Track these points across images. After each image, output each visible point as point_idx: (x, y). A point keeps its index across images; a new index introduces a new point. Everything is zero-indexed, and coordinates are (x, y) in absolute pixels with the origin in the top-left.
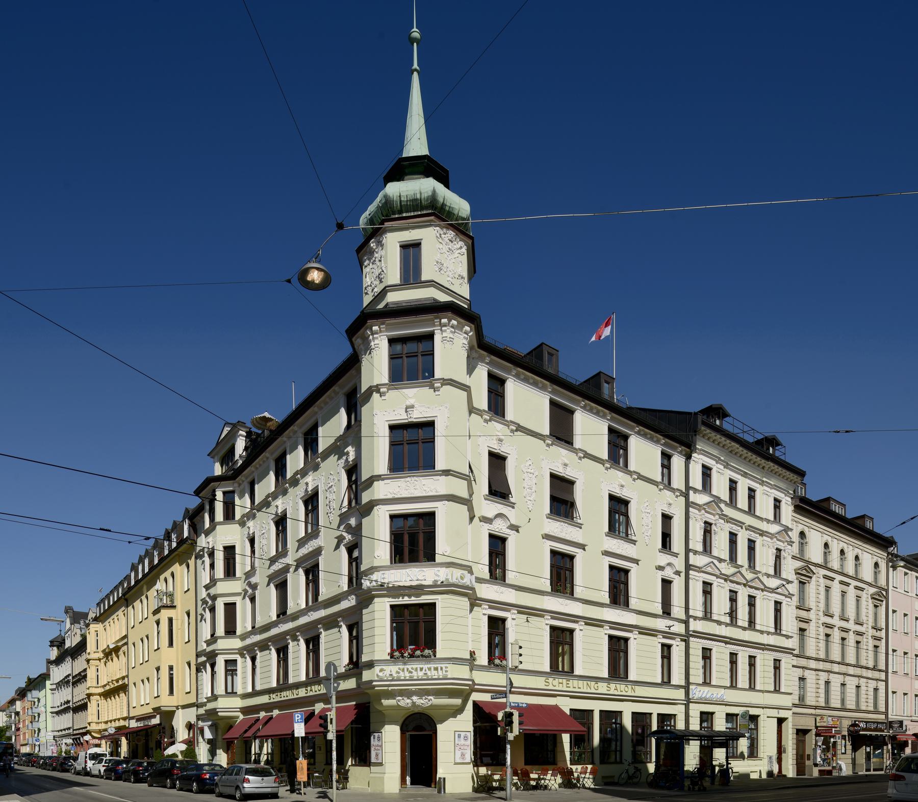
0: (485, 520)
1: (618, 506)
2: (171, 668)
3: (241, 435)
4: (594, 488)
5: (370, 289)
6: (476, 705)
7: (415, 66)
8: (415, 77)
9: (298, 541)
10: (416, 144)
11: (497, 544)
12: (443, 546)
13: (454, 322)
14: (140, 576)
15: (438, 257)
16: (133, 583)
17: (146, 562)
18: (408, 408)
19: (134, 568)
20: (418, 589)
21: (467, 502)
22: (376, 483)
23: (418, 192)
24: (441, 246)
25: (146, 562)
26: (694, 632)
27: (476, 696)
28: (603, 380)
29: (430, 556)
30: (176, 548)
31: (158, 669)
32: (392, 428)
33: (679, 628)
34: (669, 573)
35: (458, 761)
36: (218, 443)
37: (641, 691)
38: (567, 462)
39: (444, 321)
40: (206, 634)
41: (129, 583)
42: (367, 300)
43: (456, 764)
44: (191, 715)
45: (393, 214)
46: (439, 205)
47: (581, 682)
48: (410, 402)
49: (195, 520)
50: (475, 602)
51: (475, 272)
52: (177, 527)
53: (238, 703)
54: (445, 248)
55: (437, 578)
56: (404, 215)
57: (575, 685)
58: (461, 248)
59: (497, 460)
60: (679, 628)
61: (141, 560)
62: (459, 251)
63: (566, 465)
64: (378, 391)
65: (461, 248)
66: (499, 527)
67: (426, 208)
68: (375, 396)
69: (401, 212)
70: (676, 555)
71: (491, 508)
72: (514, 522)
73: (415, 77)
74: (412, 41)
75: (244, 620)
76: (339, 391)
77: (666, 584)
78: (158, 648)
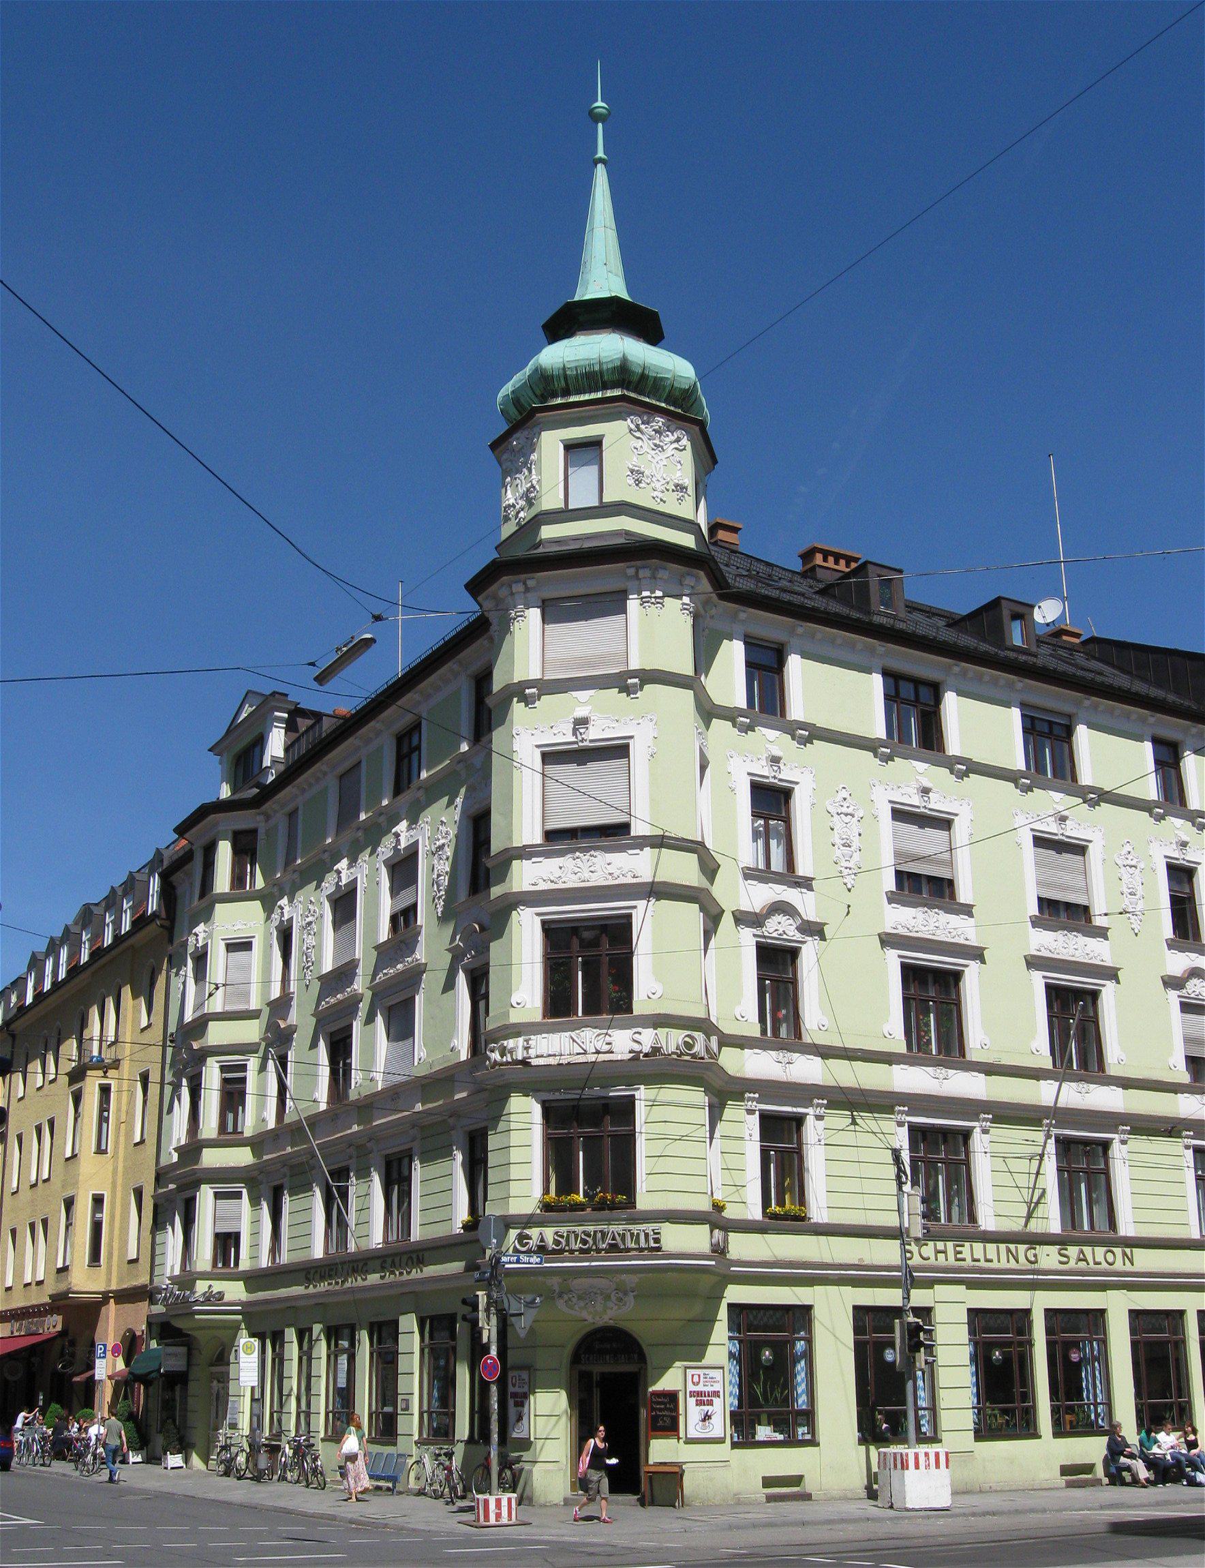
0: (742, 919)
2: (98, 1201)
3: (280, 720)
6: (736, 1310)
7: (601, 154)
8: (601, 173)
9: (377, 948)
10: (602, 277)
11: (777, 963)
14: (47, 986)
15: (634, 461)
16: (29, 999)
17: (64, 954)
18: (581, 722)
19: (36, 964)
22: (516, 864)
25: (64, 954)
27: (737, 1294)
28: (1006, 614)
30: (129, 934)
31: (69, 1203)
36: (229, 732)
37: (1146, 1260)
38: (927, 784)
40: (178, 1131)
41: (22, 996)
42: (508, 530)
44: (138, 1317)
45: (545, 400)
46: (635, 378)
47: (991, 1247)
48: (581, 712)
49: (174, 878)
50: (724, 1093)
51: (715, 462)
52: (132, 886)
53: (235, 1291)
54: (646, 445)
55: (637, 1047)
56: (573, 399)
57: (978, 1254)
58: (678, 440)
61: (53, 948)
62: (675, 445)
63: (926, 791)
65: (678, 440)
66: (780, 928)
67: (613, 386)
68: (517, 708)
72: (810, 914)
73: (601, 173)
74: (595, 118)
75: (261, 1106)
76: (452, 684)
78: (74, 1156)
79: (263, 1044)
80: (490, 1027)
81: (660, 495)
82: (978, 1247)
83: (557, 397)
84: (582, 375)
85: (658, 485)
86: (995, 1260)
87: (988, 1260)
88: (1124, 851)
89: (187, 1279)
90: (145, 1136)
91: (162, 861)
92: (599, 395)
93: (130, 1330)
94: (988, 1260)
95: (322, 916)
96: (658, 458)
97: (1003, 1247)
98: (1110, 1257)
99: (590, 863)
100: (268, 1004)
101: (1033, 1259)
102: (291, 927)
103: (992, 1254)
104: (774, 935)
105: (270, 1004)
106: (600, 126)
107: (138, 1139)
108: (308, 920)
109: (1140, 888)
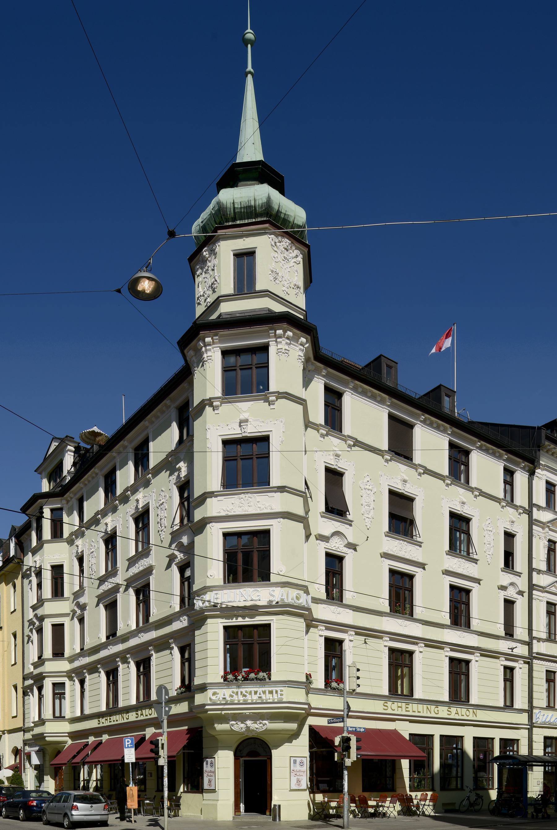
0: (321, 538)
1: (459, 524)
4: (433, 505)
5: (202, 299)
7: (250, 68)
10: (251, 150)
11: (334, 564)
12: (278, 565)
13: (290, 333)
15: (273, 266)
18: (242, 423)
20: (253, 610)
21: (303, 520)
23: (252, 199)
24: (276, 255)
26: (537, 654)
27: (312, 721)
28: (443, 394)
29: (264, 575)
32: (226, 443)
33: (522, 650)
34: (511, 593)
35: (294, 787)
36: (45, 459)
37: (482, 715)
39: (279, 332)
43: (291, 790)
46: (274, 213)
48: (243, 416)
50: (311, 624)
51: (311, 282)
59: (334, 476)
60: (522, 650)
62: (295, 260)
63: (405, 481)
64: (211, 405)
66: (337, 546)
67: (261, 215)
69: (234, 219)
70: (519, 574)
71: (325, 525)
73: (250, 78)
74: (246, 42)
76: (170, 406)
77: (509, 604)
79: (72, 613)
80: (194, 590)
81: (287, 290)
82: (415, 706)
83: (229, 222)
84: (244, 208)
85: (286, 283)
86: (422, 712)
87: (419, 712)
88: (487, 523)
89: (42, 722)
90: (17, 661)
91: (15, 530)
92: (254, 220)
93: (15, 747)
94: (419, 712)
95: (98, 548)
96: (286, 267)
97: (425, 706)
98: (468, 713)
99: (247, 502)
100: (73, 594)
101: (437, 712)
102: (83, 556)
103: (420, 709)
104: (333, 549)
105: (73, 594)
106: (249, 46)
107: (13, 663)
108: (91, 551)
109: (492, 542)
